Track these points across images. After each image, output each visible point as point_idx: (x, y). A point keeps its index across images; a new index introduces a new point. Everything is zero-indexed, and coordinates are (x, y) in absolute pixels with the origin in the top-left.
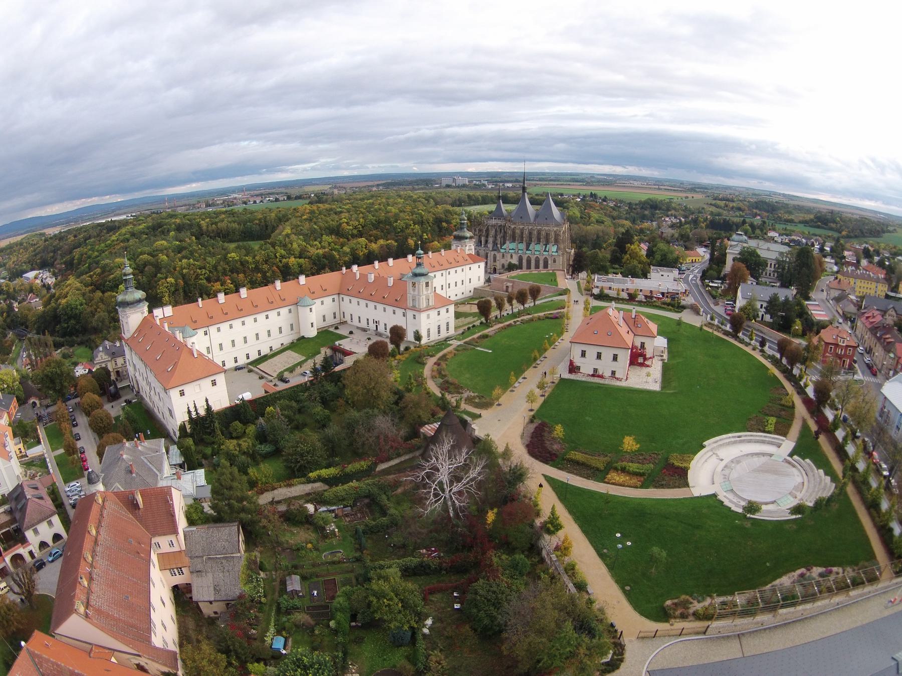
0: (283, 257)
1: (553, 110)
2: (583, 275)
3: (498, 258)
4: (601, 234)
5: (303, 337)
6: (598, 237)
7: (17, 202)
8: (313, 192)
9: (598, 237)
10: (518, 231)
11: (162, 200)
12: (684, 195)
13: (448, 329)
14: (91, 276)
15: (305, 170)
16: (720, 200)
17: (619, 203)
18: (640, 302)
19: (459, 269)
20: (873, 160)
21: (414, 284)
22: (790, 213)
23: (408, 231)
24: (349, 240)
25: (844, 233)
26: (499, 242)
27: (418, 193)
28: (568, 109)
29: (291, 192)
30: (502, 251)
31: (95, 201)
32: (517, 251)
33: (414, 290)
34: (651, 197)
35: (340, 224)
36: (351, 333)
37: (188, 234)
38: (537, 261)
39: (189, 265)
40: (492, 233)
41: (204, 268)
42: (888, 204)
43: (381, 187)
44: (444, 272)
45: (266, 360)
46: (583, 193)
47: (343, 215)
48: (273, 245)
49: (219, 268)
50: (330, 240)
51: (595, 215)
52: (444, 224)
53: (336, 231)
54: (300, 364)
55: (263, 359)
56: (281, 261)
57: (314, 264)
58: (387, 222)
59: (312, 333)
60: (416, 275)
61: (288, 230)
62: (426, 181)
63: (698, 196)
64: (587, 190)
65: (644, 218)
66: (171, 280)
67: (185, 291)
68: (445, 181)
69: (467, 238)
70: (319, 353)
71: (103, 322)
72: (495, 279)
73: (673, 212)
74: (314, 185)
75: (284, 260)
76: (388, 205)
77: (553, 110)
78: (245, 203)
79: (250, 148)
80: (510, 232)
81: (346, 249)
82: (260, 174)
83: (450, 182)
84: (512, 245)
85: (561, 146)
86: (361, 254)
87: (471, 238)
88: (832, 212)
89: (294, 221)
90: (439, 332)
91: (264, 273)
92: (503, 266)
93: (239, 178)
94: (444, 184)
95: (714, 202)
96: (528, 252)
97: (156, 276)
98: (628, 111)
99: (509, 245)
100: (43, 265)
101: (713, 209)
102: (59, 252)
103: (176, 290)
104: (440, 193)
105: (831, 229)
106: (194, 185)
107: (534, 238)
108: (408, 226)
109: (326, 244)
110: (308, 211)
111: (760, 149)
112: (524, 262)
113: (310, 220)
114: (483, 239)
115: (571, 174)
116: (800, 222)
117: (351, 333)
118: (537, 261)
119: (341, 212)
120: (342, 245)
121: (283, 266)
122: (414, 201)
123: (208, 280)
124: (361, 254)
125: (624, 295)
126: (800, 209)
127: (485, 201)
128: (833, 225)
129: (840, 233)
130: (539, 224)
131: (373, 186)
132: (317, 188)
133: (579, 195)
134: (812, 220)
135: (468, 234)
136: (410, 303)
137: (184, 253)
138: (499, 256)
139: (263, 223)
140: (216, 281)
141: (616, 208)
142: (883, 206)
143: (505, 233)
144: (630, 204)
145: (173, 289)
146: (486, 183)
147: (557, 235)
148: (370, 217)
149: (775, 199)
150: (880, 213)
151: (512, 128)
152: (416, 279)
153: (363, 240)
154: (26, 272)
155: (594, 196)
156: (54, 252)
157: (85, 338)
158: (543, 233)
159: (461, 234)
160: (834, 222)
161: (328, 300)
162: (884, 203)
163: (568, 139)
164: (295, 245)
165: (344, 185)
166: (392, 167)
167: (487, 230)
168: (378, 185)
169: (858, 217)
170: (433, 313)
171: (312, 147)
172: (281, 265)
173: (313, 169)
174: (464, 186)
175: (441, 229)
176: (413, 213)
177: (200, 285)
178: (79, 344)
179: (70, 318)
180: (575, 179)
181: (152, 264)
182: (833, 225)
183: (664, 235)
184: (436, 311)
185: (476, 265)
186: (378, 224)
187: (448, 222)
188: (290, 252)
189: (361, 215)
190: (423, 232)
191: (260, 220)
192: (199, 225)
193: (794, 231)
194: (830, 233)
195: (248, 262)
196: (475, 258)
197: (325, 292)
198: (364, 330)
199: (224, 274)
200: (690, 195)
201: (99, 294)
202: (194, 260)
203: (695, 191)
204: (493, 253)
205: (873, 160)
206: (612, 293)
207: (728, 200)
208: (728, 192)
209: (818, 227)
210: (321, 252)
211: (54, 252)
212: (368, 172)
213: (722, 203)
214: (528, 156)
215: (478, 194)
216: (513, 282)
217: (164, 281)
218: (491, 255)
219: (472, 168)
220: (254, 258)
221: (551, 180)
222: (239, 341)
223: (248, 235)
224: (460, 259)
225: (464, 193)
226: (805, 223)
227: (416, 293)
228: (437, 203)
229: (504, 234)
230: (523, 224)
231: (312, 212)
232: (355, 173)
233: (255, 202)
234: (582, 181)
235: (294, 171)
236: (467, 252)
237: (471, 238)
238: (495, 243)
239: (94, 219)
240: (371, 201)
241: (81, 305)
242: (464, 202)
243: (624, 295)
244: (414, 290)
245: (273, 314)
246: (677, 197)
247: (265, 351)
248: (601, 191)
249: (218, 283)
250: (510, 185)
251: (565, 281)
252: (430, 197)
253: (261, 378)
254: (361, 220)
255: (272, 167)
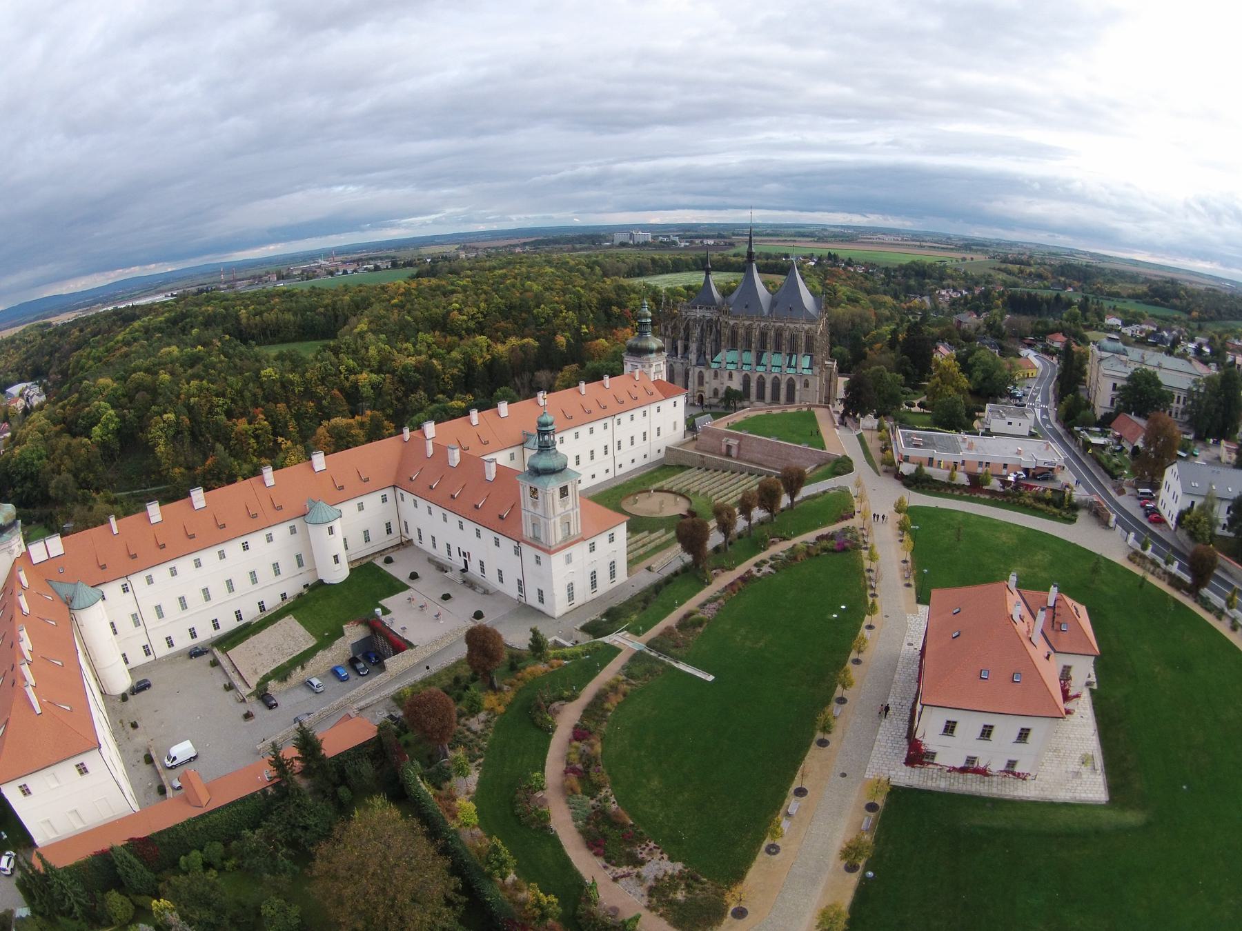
0: (351, 371)
1: (760, 137)
2: (869, 421)
3: (706, 379)
4: (858, 320)
5: (321, 583)
6: (853, 325)
7: (26, 276)
8: (429, 256)
9: (853, 325)
10: (741, 331)
11: (214, 271)
12: (959, 255)
13: (613, 575)
14: (63, 408)
15: (425, 224)
16: (1011, 263)
17: (870, 266)
18: (993, 493)
19: (638, 413)
20: (1204, 204)
21: (534, 492)
22: (1112, 282)
23: (557, 321)
24: (461, 338)
25: (1195, 314)
26: (708, 351)
27: (571, 258)
28: (780, 136)
29: (396, 257)
30: (714, 366)
31: (136, 271)
32: (739, 365)
33: (535, 505)
34: (916, 258)
35: (449, 312)
36: (414, 576)
37: (219, 331)
38: (776, 384)
39: (200, 389)
40: (696, 333)
41: (224, 396)
42: (1227, 265)
43: (527, 248)
44: (608, 421)
45: (246, 637)
46: (818, 252)
47: (454, 297)
48: (336, 351)
49: (247, 394)
50: (430, 339)
51: (843, 290)
52: (615, 308)
53: (441, 324)
54: (301, 660)
55: (244, 632)
56: (347, 379)
57: (401, 381)
58: (524, 307)
59: (338, 574)
60: (537, 472)
61: (363, 326)
62: (592, 238)
63: (980, 258)
64: (822, 249)
65: (908, 290)
66: (171, 416)
67: (192, 433)
68: (619, 238)
69: (651, 351)
70: (341, 634)
71: (64, 488)
72: (706, 431)
73: (949, 281)
74: (437, 244)
75: (352, 377)
76: (529, 278)
77: (760, 137)
78: (331, 273)
79: (347, 195)
80: (727, 332)
81: (455, 354)
82: (363, 230)
83: (626, 239)
84: (732, 356)
85: (773, 187)
86: (480, 361)
87: (660, 350)
88: (1173, 282)
89: (378, 309)
90: (594, 585)
91: (318, 400)
92: (716, 392)
93: (333, 237)
94: (617, 242)
95: (1003, 266)
96: (760, 369)
97: (148, 409)
98: (865, 137)
99: (726, 356)
100: (35, 374)
101: (1002, 276)
102: (57, 355)
103: (178, 432)
104: (611, 256)
105: (1174, 307)
106: (272, 247)
107: (770, 345)
108: (556, 313)
109: (423, 349)
110: (402, 290)
111: (1047, 189)
112: (753, 385)
113: (401, 306)
114: (680, 344)
115: (794, 226)
116: (1130, 297)
117: (414, 576)
118: (776, 384)
119: (453, 292)
120: (450, 349)
121: (351, 387)
122: (571, 270)
123: (229, 414)
124: (480, 361)
125: (962, 478)
126: (1120, 275)
127: (677, 267)
128: (1177, 302)
129: (1189, 313)
130: (779, 319)
131: (515, 246)
132: (436, 250)
133: (811, 257)
134: (1146, 294)
135: (654, 343)
136: (528, 532)
137: (199, 368)
138: (708, 375)
139: (331, 313)
140: (242, 415)
141: (867, 275)
142: (1222, 269)
143: (719, 332)
144: (887, 269)
145: (171, 432)
146: (677, 239)
147: (810, 339)
148: (497, 299)
149: (1083, 261)
150: (1223, 280)
151: (705, 162)
152: (538, 482)
153: (482, 339)
154: (12, 384)
155: (832, 257)
156: (51, 354)
157: (46, 511)
158: (787, 335)
159: (642, 344)
160: (1177, 296)
161: (372, 501)
162: (1222, 264)
163: (784, 177)
164: (373, 351)
165: (476, 245)
166: (544, 218)
167: (687, 329)
168: (525, 244)
169: (1202, 287)
170: (579, 551)
171: (432, 193)
172: (347, 384)
173: (435, 222)
174: (646, 244)
175: (609, 315)
176: (564, 291)
177: (217, 423)
178: (38, 522)
179: (25, 478)
180: (802, 233)
181: (146, 389)
182: (1177, 302)
183: (965, 326)
184: (585, 546)
185: (670, 401)
186: (508, 311)
187: (621, 305)
188: (364, 364)
189: (483, 296)
190: (581, 323)
191: (326, 306)
192: (237, 319)
193: (1142, 315)
194: (1176, 314)
195: (291, 383)
196: (666, 389)
197: (365, 485)
198: (442, 568)
199: (256, 405)
200: (968, 256)
201: (66, 439)
202: (210, 381)
203: (971, 250)
204: (697, 369)
205: (1204, 204)
206: (940, 474)
207: (1021, 263)
208: (1015, 250)
209: (1156, 304)
210: (411, 361)
211: (51, 354)
212: (513, 226)
213: (1016, 268)
214: (729, 201)
215: (667, 256)
216: (740, 438)
217: (157, 418)
218: (694, 372)
219: (656, 218)
220: (303, 375)
221: (768, 235)
222: (194, 598)
223: (307, 332)
224: (639, 392)
225: (648, 254)
226: (1136, 297)
227: (539, 511)
228: (605, 274)
229: (716, 337)
230: (751, 318)
231: (407, 293)
232: (495, 227)
233: (345, 272)
234: (811, 235)
235: (409, 226)
236: (653, 377)
237: (660, 350)
238: (701, 353)
239: (132, 298)
240: (504, 271)
241: (40, 458)
242: (647, 269)
243: (962, 478)
244: (535, 505)
245: (257, 540)
246: (952, 258)
247: (251, 614)
248: (843, 251)
249: (244, 420)
250: (711, 242)
251: (840, 440)
252: (596, 263)
253: (230, 687)
254: (482, 305)
255: (379, 220)
